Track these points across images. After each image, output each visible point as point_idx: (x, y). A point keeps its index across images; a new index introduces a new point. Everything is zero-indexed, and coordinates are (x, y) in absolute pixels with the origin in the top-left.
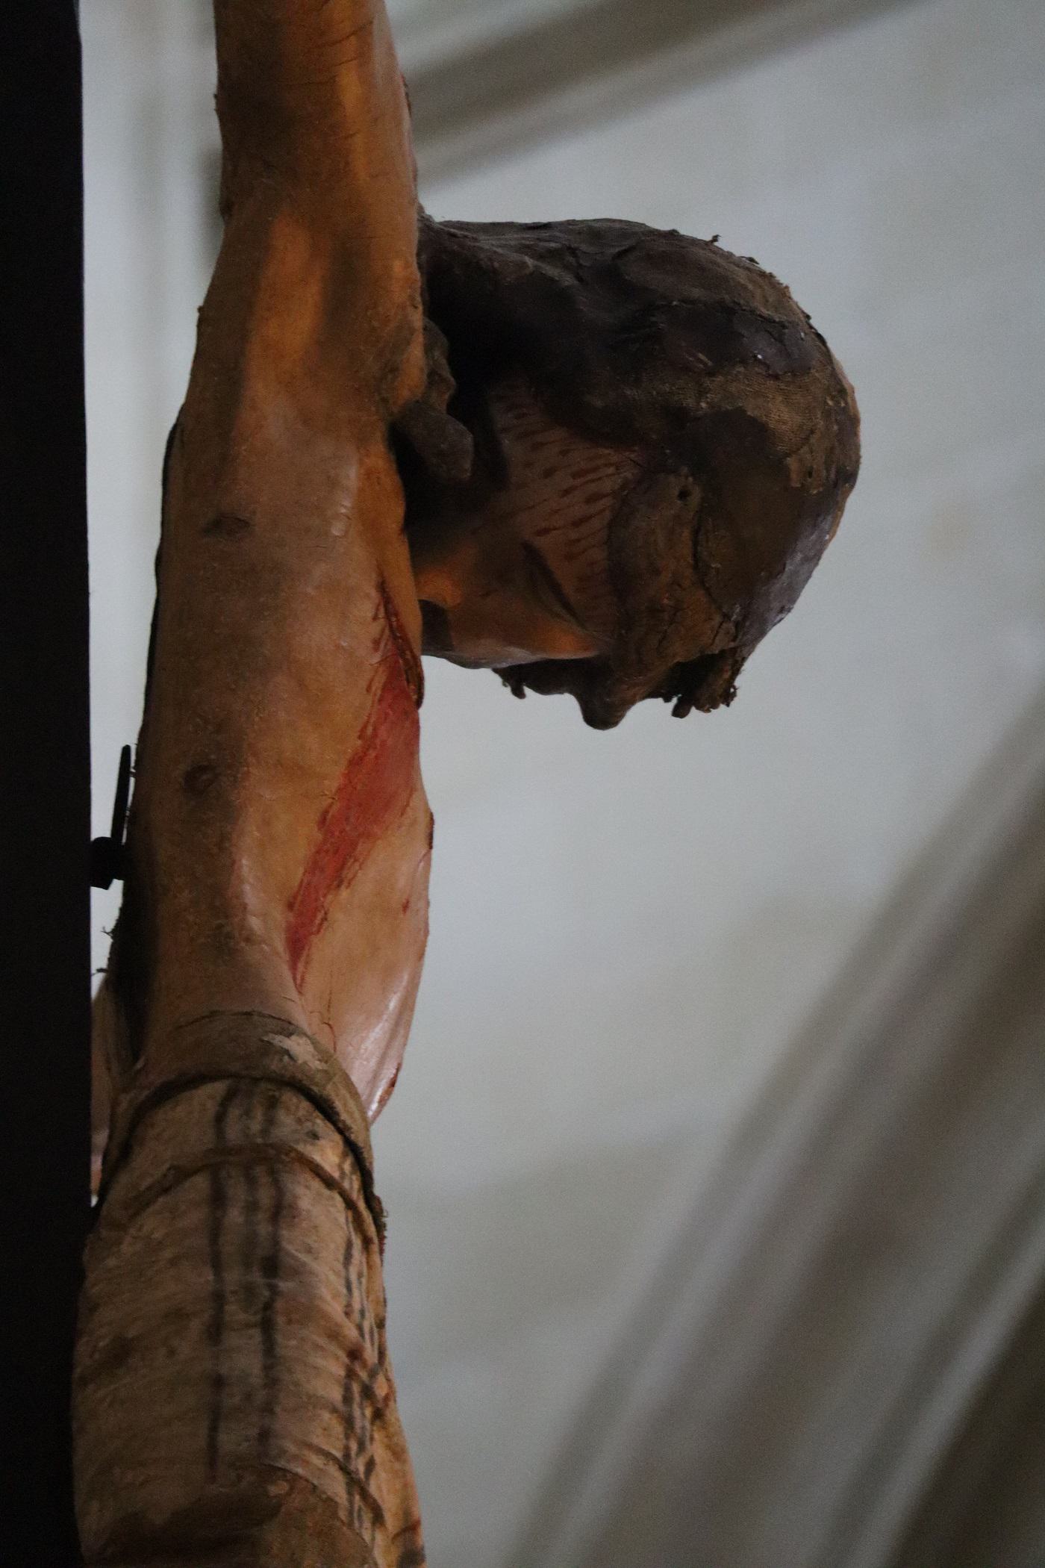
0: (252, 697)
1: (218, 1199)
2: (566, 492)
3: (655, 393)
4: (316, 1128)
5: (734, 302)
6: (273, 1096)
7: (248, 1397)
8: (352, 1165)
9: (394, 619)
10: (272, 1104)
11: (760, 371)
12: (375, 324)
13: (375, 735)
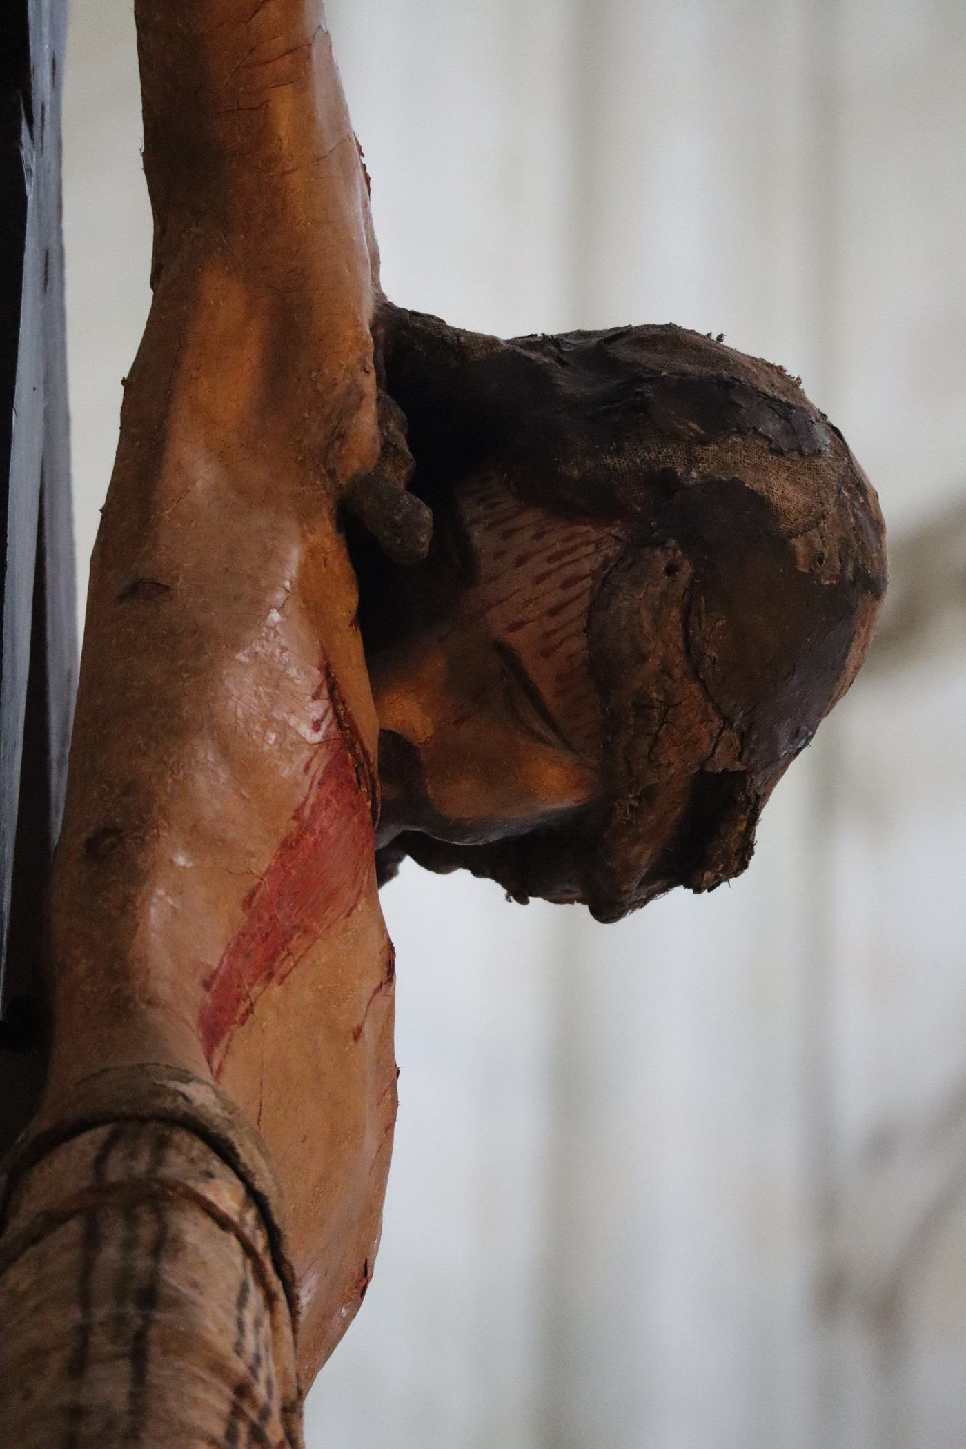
0: (166, 759)
1: (92, 1240)
2: (540, 579)
3: (638, 461)
4: (211, 1169)
5: (733, 377)
6: (163, 1136)
7: (110, 1424)
8: (256, 1219)
9: (340, 707)
10: (162, 1144)
11: (760, 444)
12: (320, 387)
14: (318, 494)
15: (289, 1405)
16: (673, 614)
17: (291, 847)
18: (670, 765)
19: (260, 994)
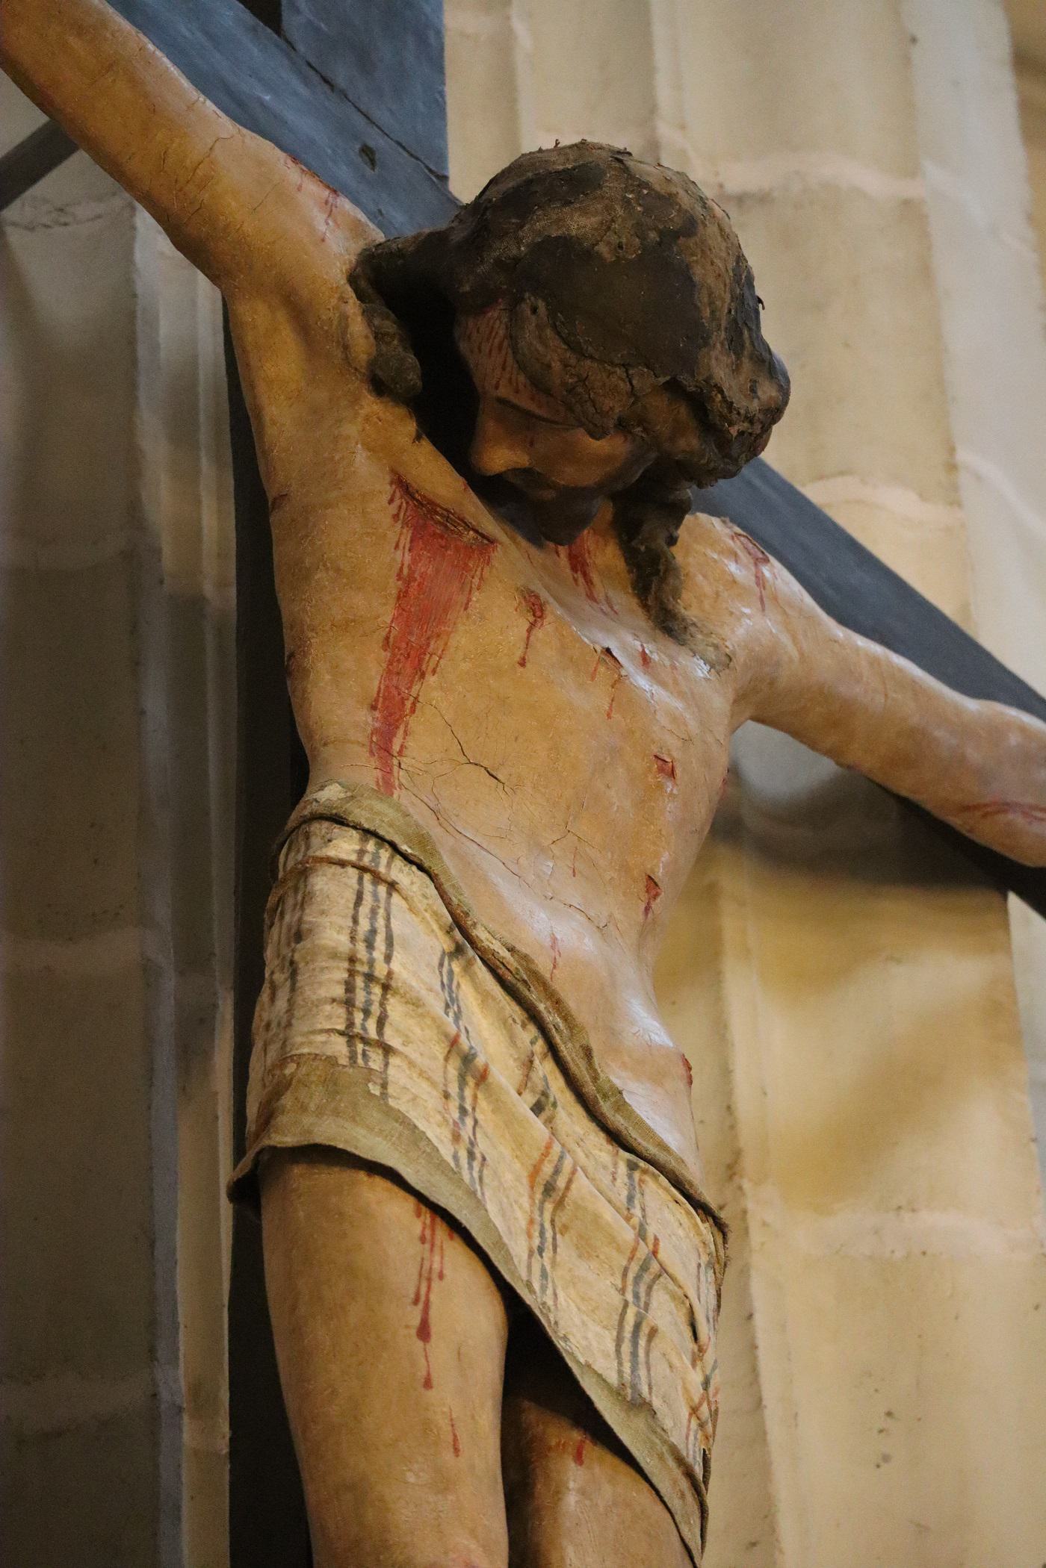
12: (326, 328)
13: (412, 572)
14: (356, 385)
15: (448, 929)
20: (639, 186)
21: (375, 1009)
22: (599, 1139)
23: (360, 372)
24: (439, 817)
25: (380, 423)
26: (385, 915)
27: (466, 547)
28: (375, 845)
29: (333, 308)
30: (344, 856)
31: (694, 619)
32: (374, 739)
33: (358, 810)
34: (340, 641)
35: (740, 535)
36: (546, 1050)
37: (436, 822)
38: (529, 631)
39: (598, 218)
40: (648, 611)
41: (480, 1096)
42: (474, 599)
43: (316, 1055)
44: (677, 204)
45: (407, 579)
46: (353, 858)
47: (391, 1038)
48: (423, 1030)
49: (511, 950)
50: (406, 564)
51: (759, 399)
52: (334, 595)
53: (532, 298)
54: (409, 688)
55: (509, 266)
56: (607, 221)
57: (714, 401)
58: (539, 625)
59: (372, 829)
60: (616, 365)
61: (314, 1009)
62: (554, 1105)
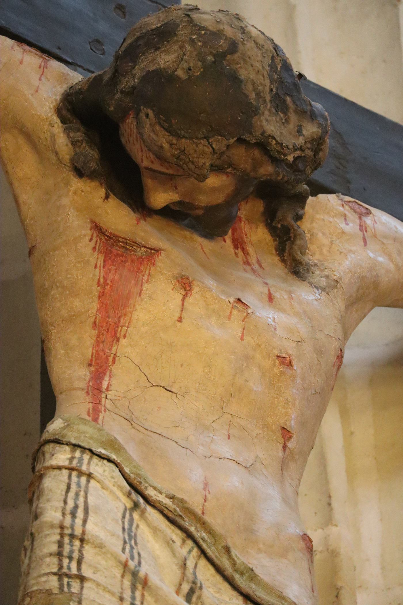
12: (44, 143)
13: (105, 279)
15: (128, 494)
16: (157, 128)
17: (103, 295)
18: (204, 164)
19: (117, 348)
20: (199, 30)
21: (76, 555)
22: (239, 601)
23: (67, 166)
24: (132, 423)
25: (83, 194)
26: (84, 495)
27: (138, 259)
28: (80, 453)
29: (46, 131)
30: (61, 463)
31: (316, 262)
32: (91, 384)
33: (71, 433)
34: (68, 329)
35: (350, 202)
36: (200, 554)
37: (131, 427)
38: (183, 300)
39: (176, 54)
40: (285, 263)
41: (146, 594)
42: (145, 289)
43: (41, 590)
44: (224, 35)
45: (103, 284)
46: (66, 463)
47: (86, 572)
48: (106, 561)
49: (172, 497)
50: (102, 275)
51: (304, 135)
52: (62, 302)
53: (145, 109)
54: (111, 349)
55: (132, 92)
56: (180, 56)
57: (271, 144)
58: (189, 295)
59: (77, 443)
60: (200, 139)
61: (41, 561)
62: (201, 588)
